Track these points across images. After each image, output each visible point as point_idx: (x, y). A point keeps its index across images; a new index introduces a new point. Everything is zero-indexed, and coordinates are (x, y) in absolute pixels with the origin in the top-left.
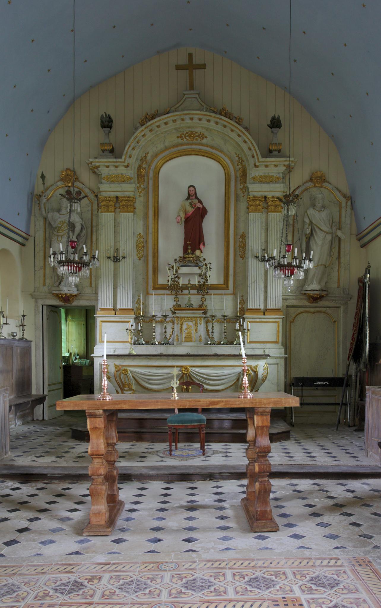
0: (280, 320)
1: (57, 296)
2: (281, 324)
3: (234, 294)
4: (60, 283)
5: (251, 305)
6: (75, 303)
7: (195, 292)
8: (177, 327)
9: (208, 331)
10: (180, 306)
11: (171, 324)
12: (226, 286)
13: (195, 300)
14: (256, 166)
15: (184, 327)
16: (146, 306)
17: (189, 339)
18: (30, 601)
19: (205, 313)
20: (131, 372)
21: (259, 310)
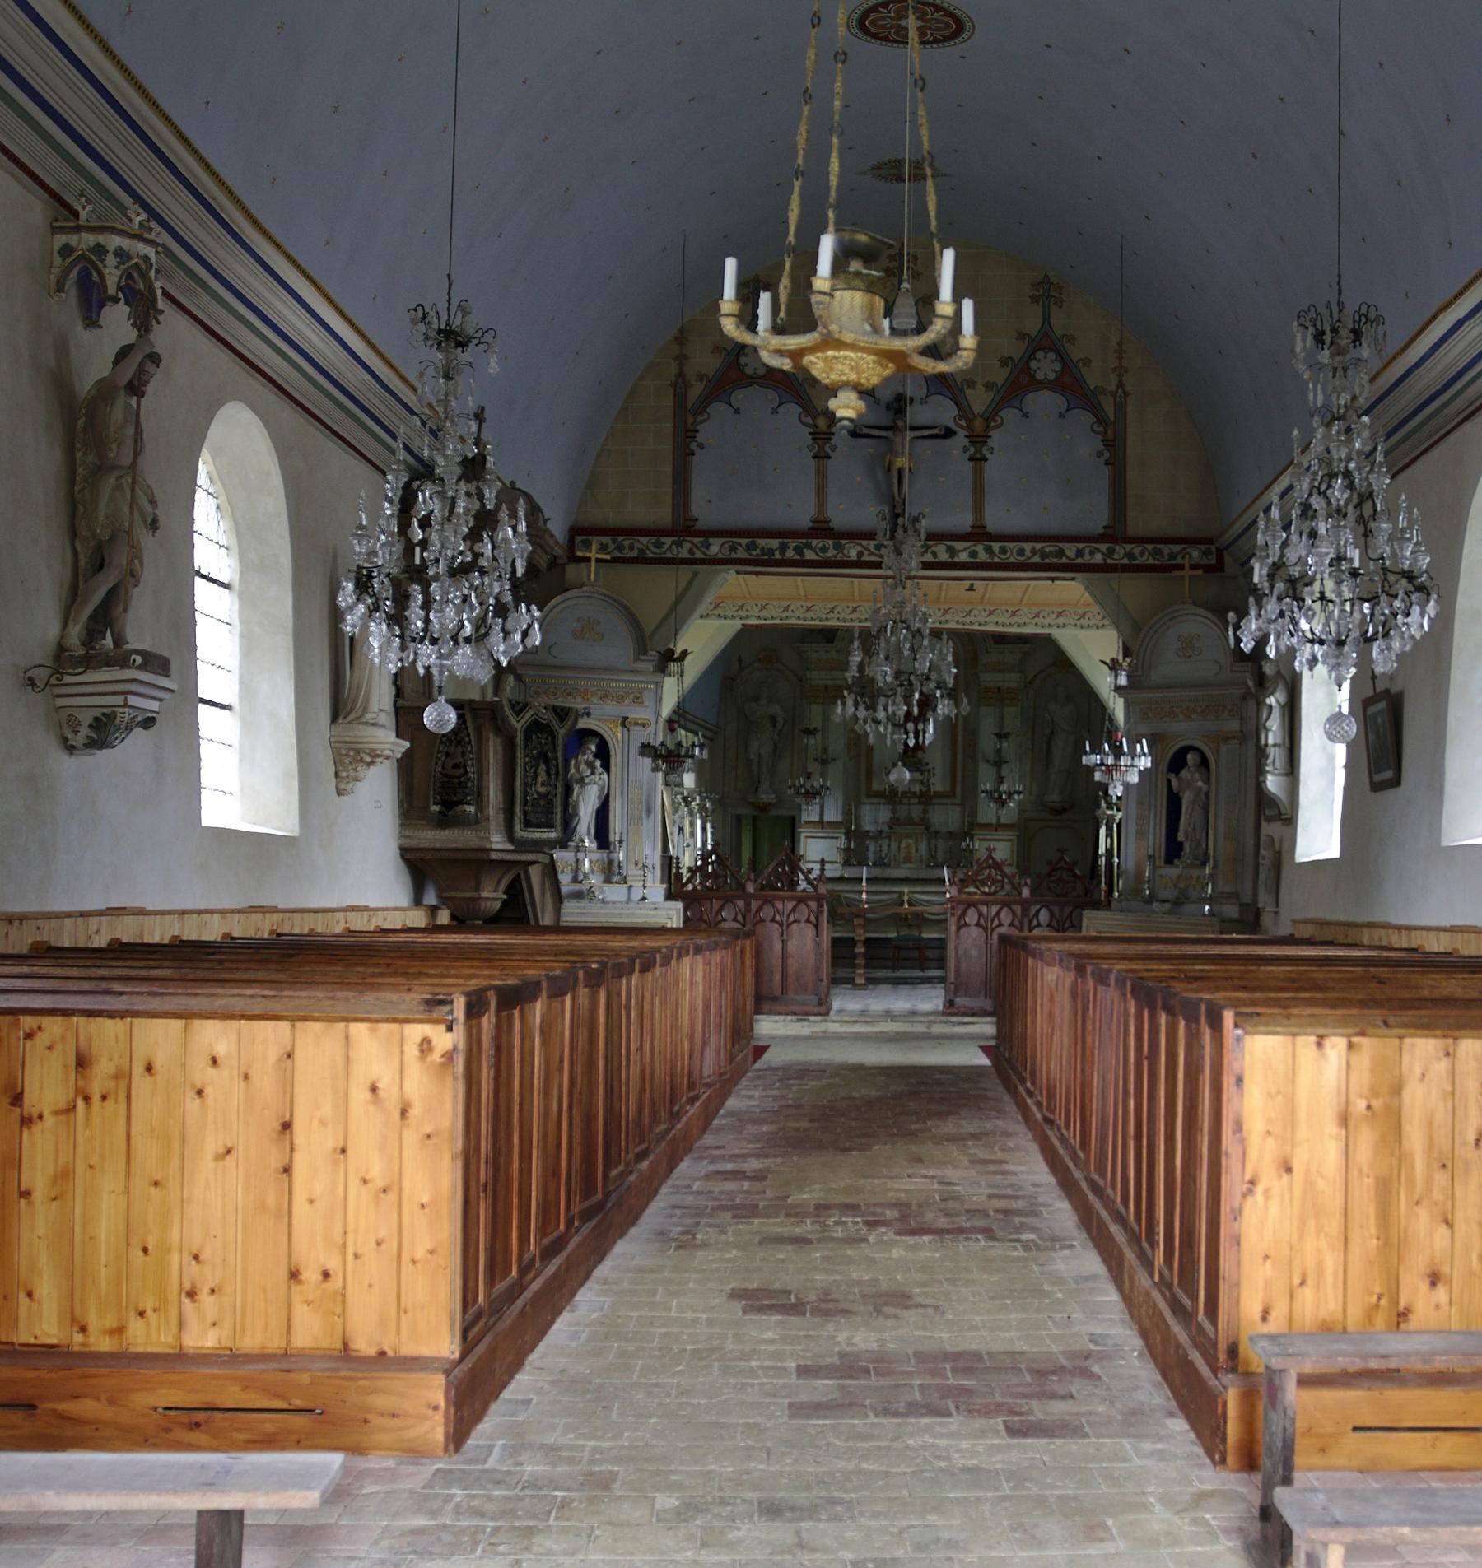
0: (1014, 838)
1: (753, 805)
2: (1015, 842)
3: (962, 804)
4: (757, 789)
5: (981, 820)
6: (773, 812)
7: (916, 800)
8: (894, 845)
9: (930, 849)
10: (898, 819)
11: (887, 841)
12: (952, 794)
13: (916, 811)
14: (987, 652)
15: (903, 845)
16: (858, 817)
17: (908, 859)
18: (491, 1282)
19: (927, 828)
20: (846, 898)
21: (991, 825)
